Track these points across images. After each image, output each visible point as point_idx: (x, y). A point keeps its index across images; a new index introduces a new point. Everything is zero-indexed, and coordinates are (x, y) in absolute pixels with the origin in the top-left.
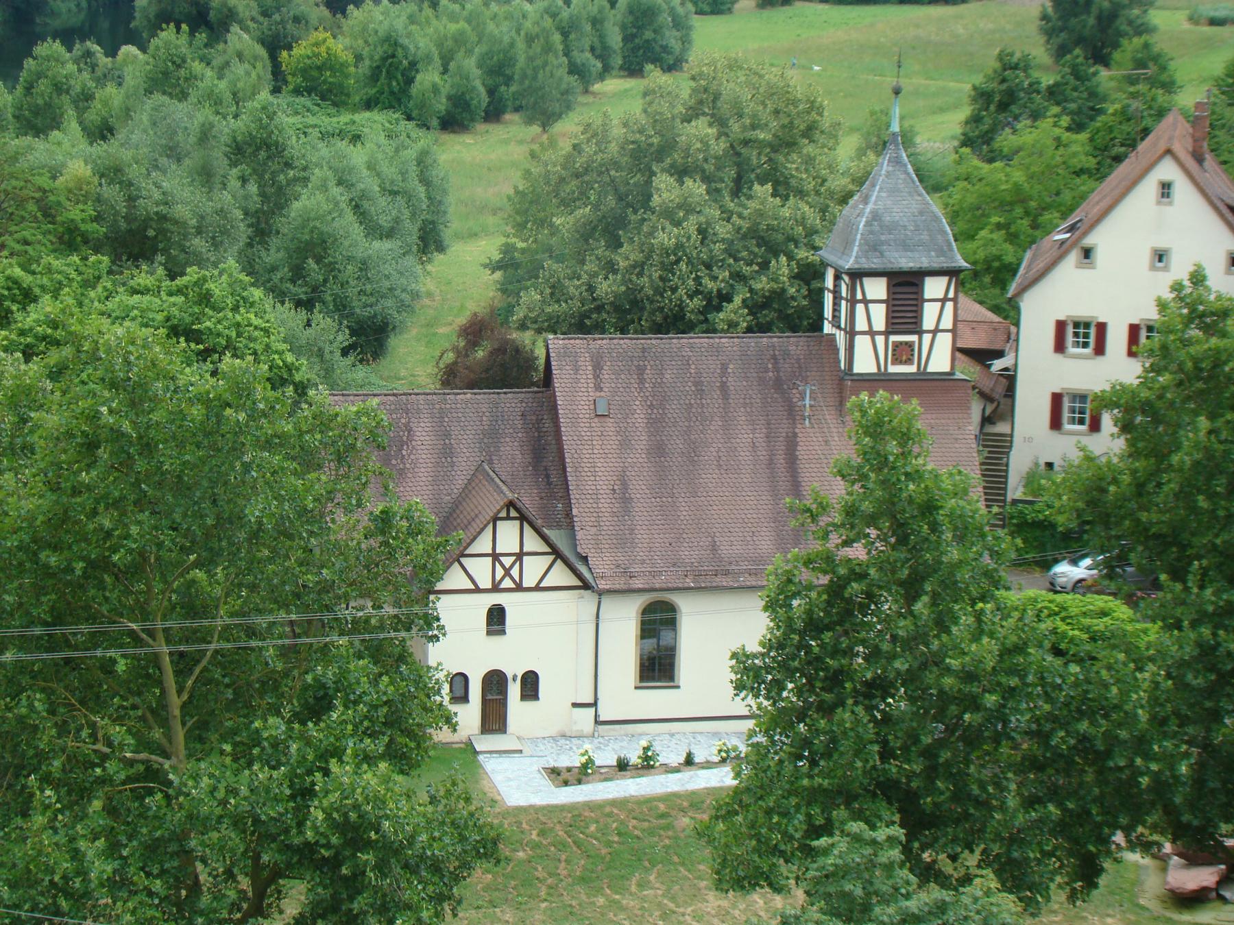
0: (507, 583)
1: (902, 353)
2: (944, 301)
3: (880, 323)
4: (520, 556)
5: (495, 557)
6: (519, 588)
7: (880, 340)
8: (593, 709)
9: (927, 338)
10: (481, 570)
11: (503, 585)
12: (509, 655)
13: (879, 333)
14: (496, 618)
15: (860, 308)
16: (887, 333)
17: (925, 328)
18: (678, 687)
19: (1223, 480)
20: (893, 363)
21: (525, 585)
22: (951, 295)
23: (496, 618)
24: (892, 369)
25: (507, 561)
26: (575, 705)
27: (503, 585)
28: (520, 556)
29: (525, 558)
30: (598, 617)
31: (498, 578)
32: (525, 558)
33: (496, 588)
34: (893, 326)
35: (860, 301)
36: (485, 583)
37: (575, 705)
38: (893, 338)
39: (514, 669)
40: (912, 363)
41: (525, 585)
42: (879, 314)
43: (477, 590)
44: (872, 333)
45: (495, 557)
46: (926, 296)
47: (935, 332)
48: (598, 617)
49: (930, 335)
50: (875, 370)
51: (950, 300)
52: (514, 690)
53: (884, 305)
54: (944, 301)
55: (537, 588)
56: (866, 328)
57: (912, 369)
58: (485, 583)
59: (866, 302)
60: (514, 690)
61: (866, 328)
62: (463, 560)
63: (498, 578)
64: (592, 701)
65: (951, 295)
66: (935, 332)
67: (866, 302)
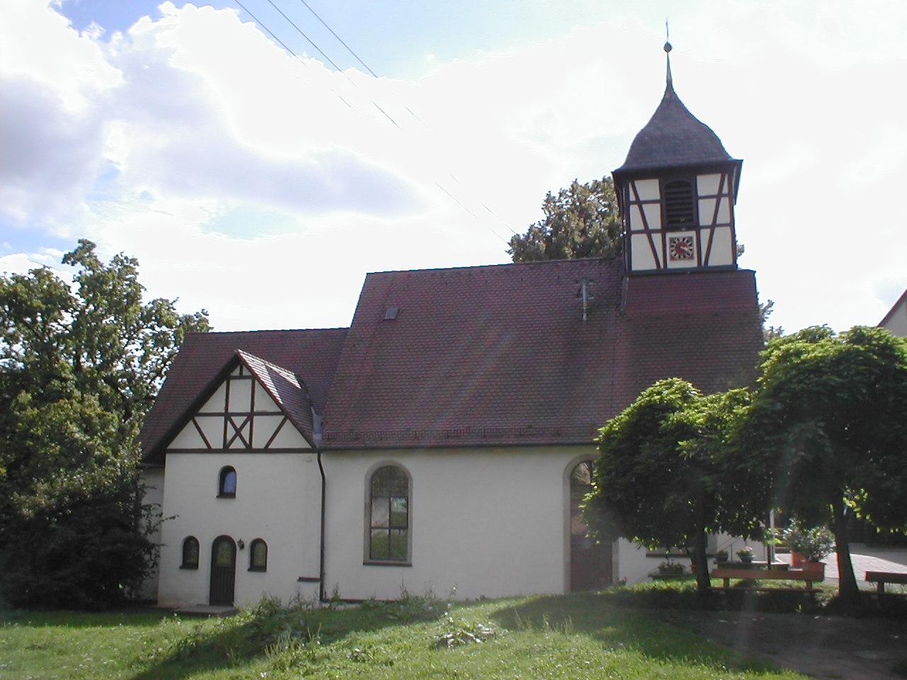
0: (238, 444)
1: (680, 250)
2: (719, 197)
3: (655, 220)
4: (250, 416)
5: (228, 416)
6: (249, 449)
7: (657, 238)
8: (318, 585)
9: (705, 234)
10: (214, 429)
11: (232, 447)
12: (238, 521)
13: (656, 231)
14: (226, 485)
15: (634, 209)
16: (664, 231)
17: (702, 223)
18: (410, 565)
19: (858, 514)
20: (672, 258)
21: (254, 446)
22: (725, 190)
23: (226, 485)
24: (672, 265)
25: (238, 421)
26: (301, 579)
27: (232, 447)
28: (250, 416)
29: (230, 411)
30: (324, 478)
31: (229, 438)
32: (230, 411)
33: (226, 449)
34: (670, 223)
35: (633, 203)
36: (217, 443)
37: (301, 579)
38: (669, 235)
39: (243, 534)
40: (692, 257)
41: (254, 446)
42: (654, 216)
43: (209, 450)
44: (648, 232)
45: (228, 416)
46: (700, 194)
47: (713, 226)
48: (324, 478)
49: (708, 231)
50: (654, 267)
51: (725, 195)
52: (243, 559)
53: (658, 206)
54: (719, 197)
55: (266, 450)
56: (642, 227)
57: (693, 264)
58: (217, 443)
59: (639, 203)
60: (243, 559)
61: (642, 227)
62: (197, 419)
63: (229, 438)
64: (318, 576)
65: (725, 190)
66: (713, 226)
67: (639, 203)
